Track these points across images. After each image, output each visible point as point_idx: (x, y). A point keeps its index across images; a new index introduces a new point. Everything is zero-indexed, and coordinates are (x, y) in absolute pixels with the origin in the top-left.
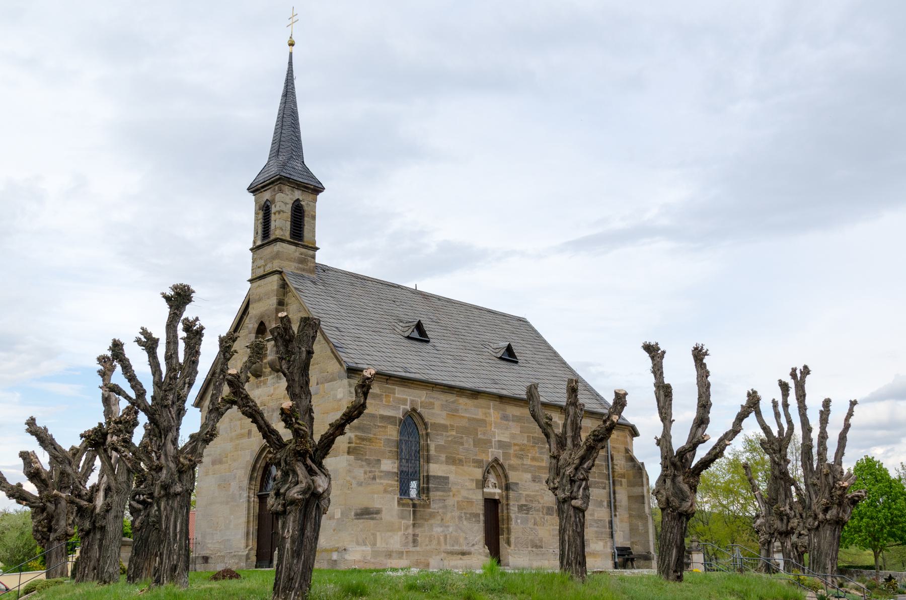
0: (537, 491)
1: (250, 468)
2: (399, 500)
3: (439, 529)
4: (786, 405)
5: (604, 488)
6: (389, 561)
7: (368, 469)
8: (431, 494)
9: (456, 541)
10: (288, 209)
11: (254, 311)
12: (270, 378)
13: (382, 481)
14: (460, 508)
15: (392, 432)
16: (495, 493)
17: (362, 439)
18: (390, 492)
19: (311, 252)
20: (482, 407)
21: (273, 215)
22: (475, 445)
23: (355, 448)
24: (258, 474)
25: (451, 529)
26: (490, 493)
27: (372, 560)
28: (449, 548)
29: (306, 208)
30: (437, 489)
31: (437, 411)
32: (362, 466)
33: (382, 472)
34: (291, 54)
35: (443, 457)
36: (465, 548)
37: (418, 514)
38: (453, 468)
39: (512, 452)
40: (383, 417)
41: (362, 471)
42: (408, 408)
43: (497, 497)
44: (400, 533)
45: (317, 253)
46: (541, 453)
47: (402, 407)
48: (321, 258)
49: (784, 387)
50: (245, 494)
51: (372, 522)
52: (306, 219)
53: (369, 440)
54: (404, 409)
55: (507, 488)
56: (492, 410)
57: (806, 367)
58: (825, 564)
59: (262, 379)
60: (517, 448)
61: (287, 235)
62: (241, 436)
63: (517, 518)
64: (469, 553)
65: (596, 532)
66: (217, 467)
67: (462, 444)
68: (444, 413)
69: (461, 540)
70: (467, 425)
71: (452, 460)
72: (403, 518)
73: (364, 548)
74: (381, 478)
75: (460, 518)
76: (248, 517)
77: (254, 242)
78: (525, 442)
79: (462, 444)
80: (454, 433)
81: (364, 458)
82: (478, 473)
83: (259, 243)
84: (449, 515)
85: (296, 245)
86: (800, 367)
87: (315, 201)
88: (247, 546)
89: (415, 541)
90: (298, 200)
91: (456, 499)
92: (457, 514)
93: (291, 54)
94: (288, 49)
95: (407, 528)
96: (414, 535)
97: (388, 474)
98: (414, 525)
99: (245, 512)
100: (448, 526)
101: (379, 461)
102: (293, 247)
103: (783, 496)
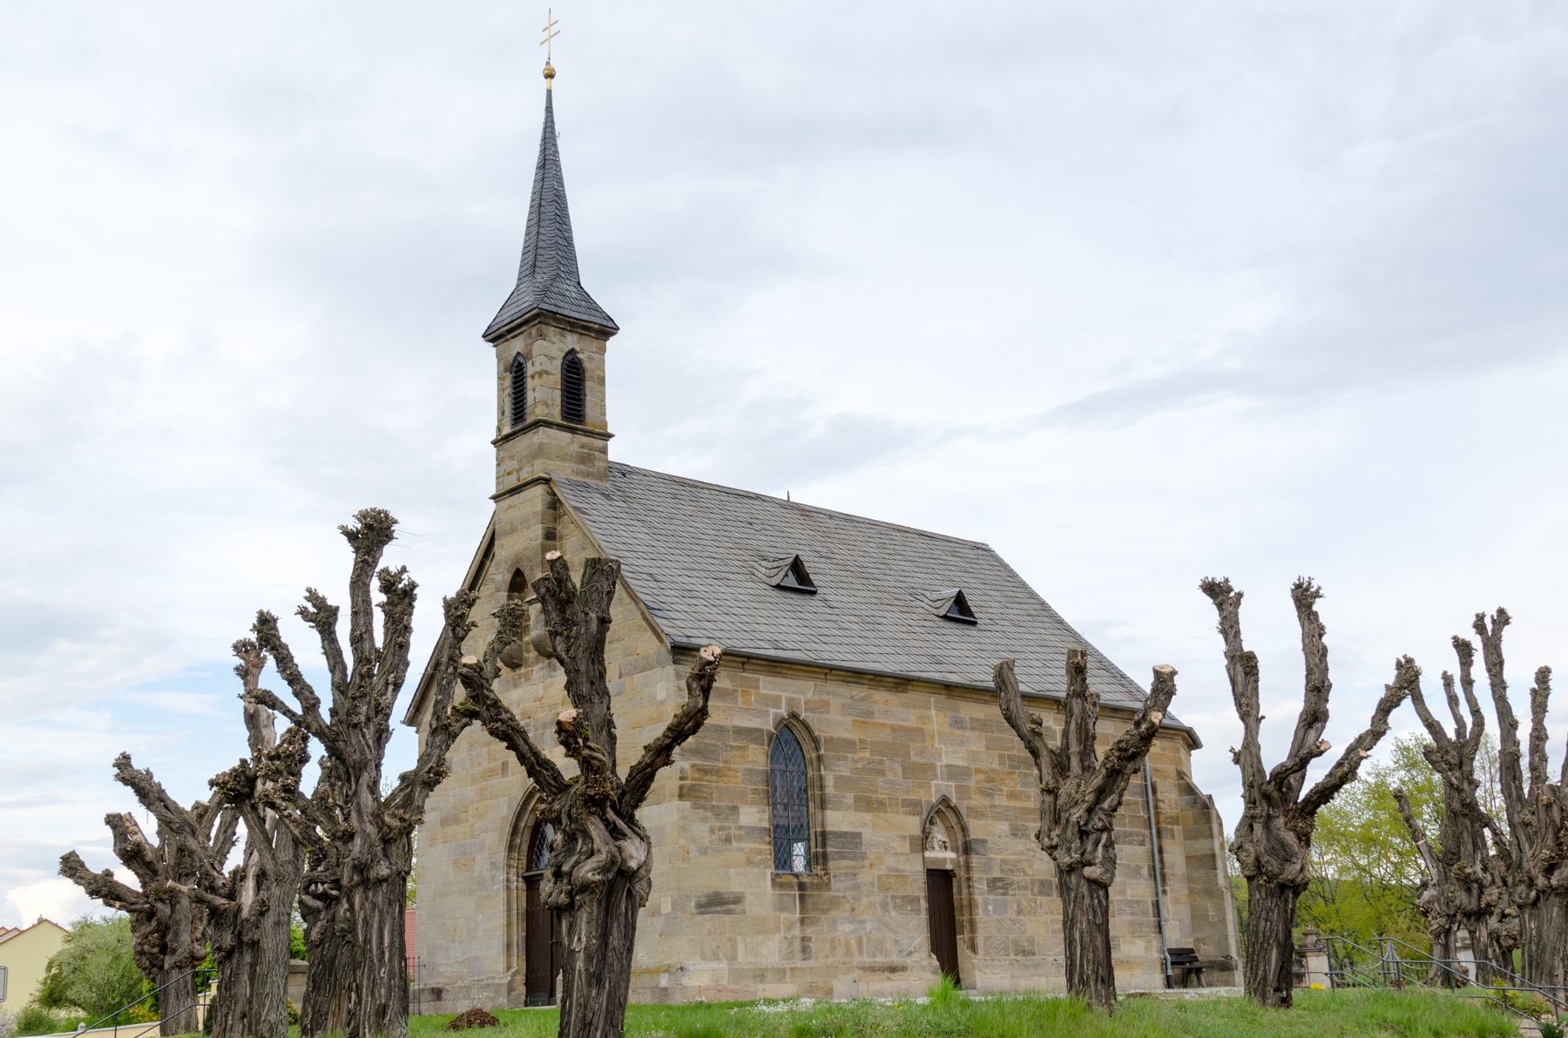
0: (1022, 853)
1: (508, 829)
2: (775, 877)
3: (848, 927)
4: (1468, 682)
5: (1142, 844)
6: (761, 986)
7: (717, 824)
8: (831, 864)
9: (879, 948)
10: (556, 367)
11: (502, 551)
12: (536, 668)
13: (743, 845)
14: (884, 887)
15: (757, 757)
16: (945, 860)
17: (705, 771)
18: (757, 865)
19: (599, 443)
20: (914, 707)
21: (529, 380)
22: (905, 776)
23: (692, 788)
24: (523, 840)
25: (869, 926)
26: (937, 860)
27: (731, 986)
28: (867, 960)
29: (587, 365)
30: (841, 856)
31: (834, 716)
32: (705, 820)
33: (740, 828)
34: (549, 92)
35: (849, 798)
36: (896, 959)
37: (809, 901)
38: (868, 817)
39: (972, 783)
40: (740, 732)
41: (706, 827)
42: (783, 712)
43: (949, 867)
44: (779, 937)
45: (611, 443)
46: (1025, 785)
47: (772, 711)
48: (617, 452)
49: (1463, 649)
50: (502, 876)
51: (727, 918)
52: (588, 384)
53: (717, 772)
54: (776, 714)
55: (967, 849)
56: (933, 712)
57: (1501, 612)
58: (1552, 968)
59: (523, 670)
60: (981, 777)
61: (556, 415)
62: (491, 773)
63: (986, 904)
64: (904, 968)
65: (1131, 923)
66: (449, 829)
67: (882, 773)
68: (849, 719)
69: (888, 945)
70: (890, 739)
71: (865, 803)
72: (782, 909)
73: (715, 965)
74: (739, 838)
75: (884, 905)
76: (509, 916)
77: (499, 430)
78: (996, 766)
79: (882, 773)
80: (867, 755)
81: (709, 804)
82: (914, 825)
83: (507, 430)
84: (864, 901)
85: (573, 430)
86: (1490, 612)
87: (603, 351)
88: (509, 968)
89: (805, 950)
90: (572, 351)
91: (876, 872)
92: (878, 898)
93: (549, 92)
94: (545, 83)
95: (789, 928)
96: (803, 939)
97: (752, 831)
98: (802, 921)
99: (502, 909)
100: (863, 922)
101: (735, 809)
102: (568, 436)
103: (1470, 847)
